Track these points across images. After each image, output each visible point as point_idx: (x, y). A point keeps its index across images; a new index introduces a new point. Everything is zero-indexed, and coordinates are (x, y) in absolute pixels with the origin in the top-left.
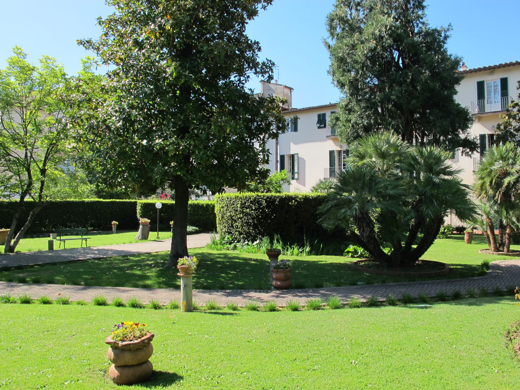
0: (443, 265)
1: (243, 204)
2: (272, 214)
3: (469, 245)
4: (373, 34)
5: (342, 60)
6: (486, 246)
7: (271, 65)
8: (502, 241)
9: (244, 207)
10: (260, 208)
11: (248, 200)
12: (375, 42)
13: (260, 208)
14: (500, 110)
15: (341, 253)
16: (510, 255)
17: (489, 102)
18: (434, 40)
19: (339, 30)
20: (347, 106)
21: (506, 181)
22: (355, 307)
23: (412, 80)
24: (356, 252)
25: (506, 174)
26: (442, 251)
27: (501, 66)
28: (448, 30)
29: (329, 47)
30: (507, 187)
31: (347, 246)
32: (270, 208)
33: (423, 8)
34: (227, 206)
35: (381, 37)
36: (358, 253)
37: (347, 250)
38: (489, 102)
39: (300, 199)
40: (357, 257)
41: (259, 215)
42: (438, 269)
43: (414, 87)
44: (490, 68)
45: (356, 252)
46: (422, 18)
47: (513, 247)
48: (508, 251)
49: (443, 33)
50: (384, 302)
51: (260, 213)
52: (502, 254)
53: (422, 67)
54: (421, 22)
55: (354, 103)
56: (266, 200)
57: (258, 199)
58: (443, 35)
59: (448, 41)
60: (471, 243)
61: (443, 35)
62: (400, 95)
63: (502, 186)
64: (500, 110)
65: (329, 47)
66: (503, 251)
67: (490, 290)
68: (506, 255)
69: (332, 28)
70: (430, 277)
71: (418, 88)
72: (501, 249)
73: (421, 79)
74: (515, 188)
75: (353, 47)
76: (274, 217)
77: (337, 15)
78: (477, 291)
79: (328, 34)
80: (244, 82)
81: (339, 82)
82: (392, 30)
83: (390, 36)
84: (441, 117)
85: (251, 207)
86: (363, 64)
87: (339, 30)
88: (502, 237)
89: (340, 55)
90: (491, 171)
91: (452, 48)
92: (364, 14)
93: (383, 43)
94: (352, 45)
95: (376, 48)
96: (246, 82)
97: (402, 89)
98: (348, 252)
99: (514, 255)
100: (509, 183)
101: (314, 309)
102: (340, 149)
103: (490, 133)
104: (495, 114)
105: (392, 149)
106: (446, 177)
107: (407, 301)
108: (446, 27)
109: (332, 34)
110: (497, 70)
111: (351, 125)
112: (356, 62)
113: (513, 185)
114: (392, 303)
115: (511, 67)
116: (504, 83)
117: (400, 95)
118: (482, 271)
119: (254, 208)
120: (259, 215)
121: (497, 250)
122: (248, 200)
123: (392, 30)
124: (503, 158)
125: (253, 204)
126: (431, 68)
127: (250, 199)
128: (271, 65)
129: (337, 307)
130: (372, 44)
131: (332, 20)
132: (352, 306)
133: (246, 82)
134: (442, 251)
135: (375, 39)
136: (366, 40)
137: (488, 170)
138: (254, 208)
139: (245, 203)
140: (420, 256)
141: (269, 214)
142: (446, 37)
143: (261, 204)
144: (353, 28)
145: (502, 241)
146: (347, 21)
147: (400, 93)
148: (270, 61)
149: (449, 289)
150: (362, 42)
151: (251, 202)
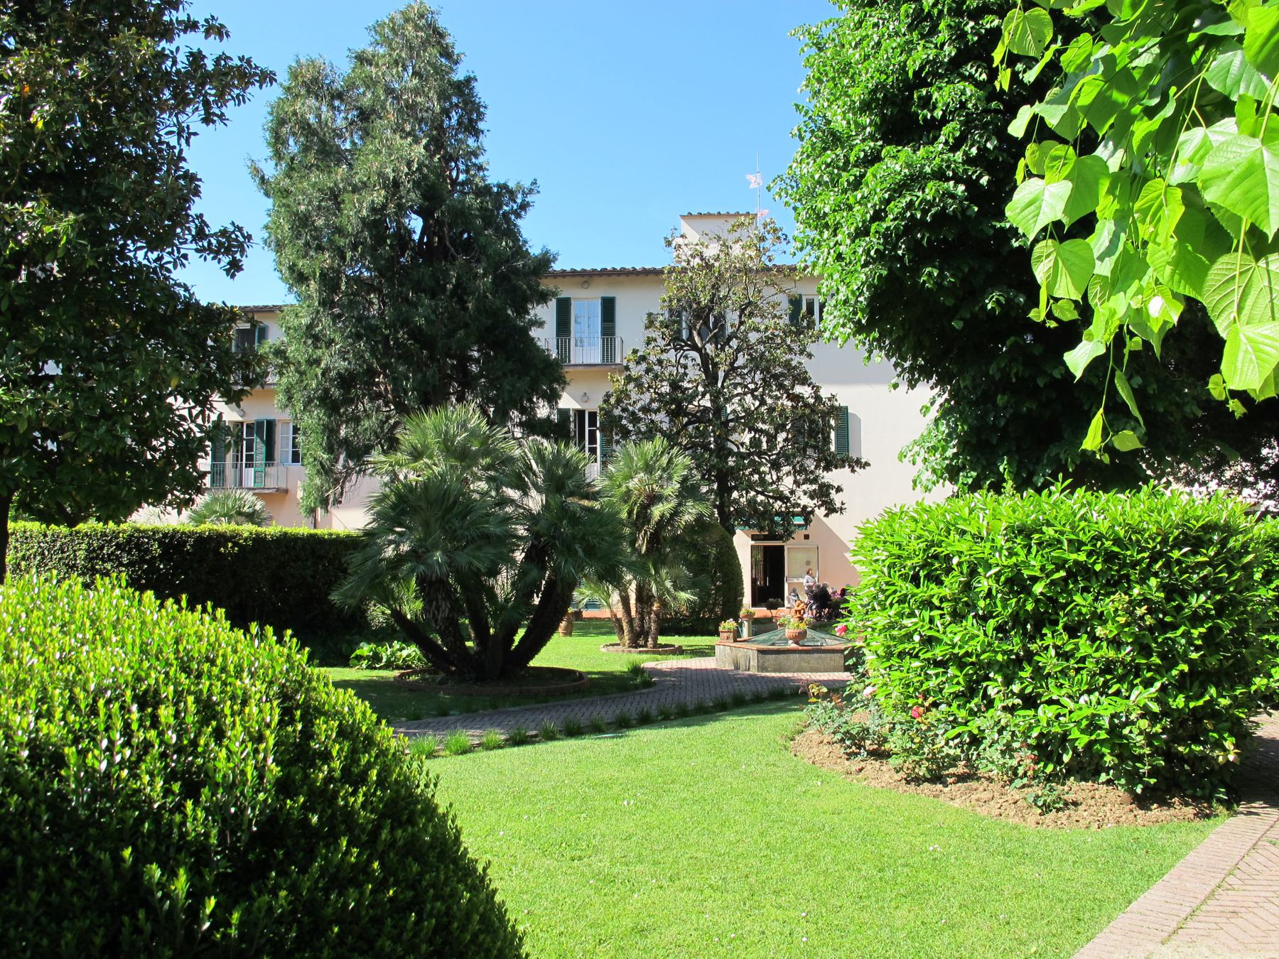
0: (581, 676)
1: (94, 550)
2: (176, 576)
3: (569, 638)
4: (380, 174)
5: (302, 222)
6: (615, 639)
7: (241, 239)
8: (642, 626)
9: (97, 558)
10: (142, 560)
11: (111, 541)
12: (383, 192)
13: (142, 560)
14: (599, 361)
15: (344, 661)
16: (660, 653)
17: (580, 343)
18: (499, 209)
19: (293, 147)
20: (310, 327)
21: (657, 511)
22: (494, 748)
23: (456, 287)
24: (376, 658)
25: (655, 498)
26: (561, 652)
27: (604, 273)
28: (531, 191)
29: (263, 180)
30: (658, 523)
31: (354, 645)
32: (171, 559)
33: (477, 133)
34: (43, 554)
35: (396, 184)
36: (380, 660)
37: (358, 652)
38: (580, 343)
39: (246, 540)
40: (380, 668)
41: (140, 577)
42: (568, 684)
43: (463, 303)
44: (583, 273)
45: (376, 658)
46: (476, 157)
47: (662, 640)
48: (656, 645)
49: (520, 196)
50: (536, 736)
51: (144, 571)
52: (647, 652)
53: (478, 261)
54: (475, 165)
55: (326, 320)
56: (161, 543)
57: (138, 538)
58: (519, 201)
59: (530, 215)
60: (570, 635)
61: (519, 201)
62: (433, 317)
63: (649, 522)
64: (599, 361)
65: (263, 180)
66: (645, 646)
67: (691, 707)
68: (654, 653)
69: (278, 141)
70: (563, 694)
71: (470, 305)
72: (641, 642)
73: (478, 289)
74: (672, 526)
75: (335, 196)
76: (182, 581)
77: (295, 114)
78: (654, 712)
79: (269, 152)
80: (170, 266)
81: (292, 268)
82: (421, 173)
83: (417, 184)
84: (512, 372)
85: (118, 558)
86: (356, 236)
87: (293, 147)
88: (642, 619)
89: (303, 208)
90: (629, 491)
91: (536, 233)
92: (346, 118)
93: (401, 198)
94: (331, 189)
95: (384, 206)
96: (175, 267)
97: (437, 305)
98: (359, 658)
99: (666, 653)
100: (662, 516)
101: (457, 753)
102: (240, 419)
103: (578, 407)
104: (590, 369)
105: (476, 443)
106: (586, 503)
107: (573, 732)
108: (527, 184)
109: (278, 156)
110: (597, 279)
111: (319, 372)
112: (339, 230)
113: (669, 520)
114: (550, 737)
115: (622, 278)
116: (608, 307)
117: (433, 317)
118: (636, 681)
119: (125, 561)
120: (140, 577)
121: (634, 644)
122: (111, 541)
123: (421, 173)
124: (649, 469)
125: (123, 550)
126: (493, 268)
127: (117, 537)
128: (241, 239)
129: (464, 752)
130: (378, 196)
131: (282, 122)
132: (488, 747)
133: (175, 267)
134: (561, 652)
135: (385, 187)
136: (364, 183)
137: (623, 489)
138: (125, 561)
139: (102, 548)
140: (532, 658)
141: (167, 574)
142: (524, 206)
143: (147, 551)
144: (324, 150)
145: (642, 626)
146: (315, 133)
147: (434, 312)
148: (240, 229)
149: (606, 712)
150: (355, 190)
151: (118, 546)
